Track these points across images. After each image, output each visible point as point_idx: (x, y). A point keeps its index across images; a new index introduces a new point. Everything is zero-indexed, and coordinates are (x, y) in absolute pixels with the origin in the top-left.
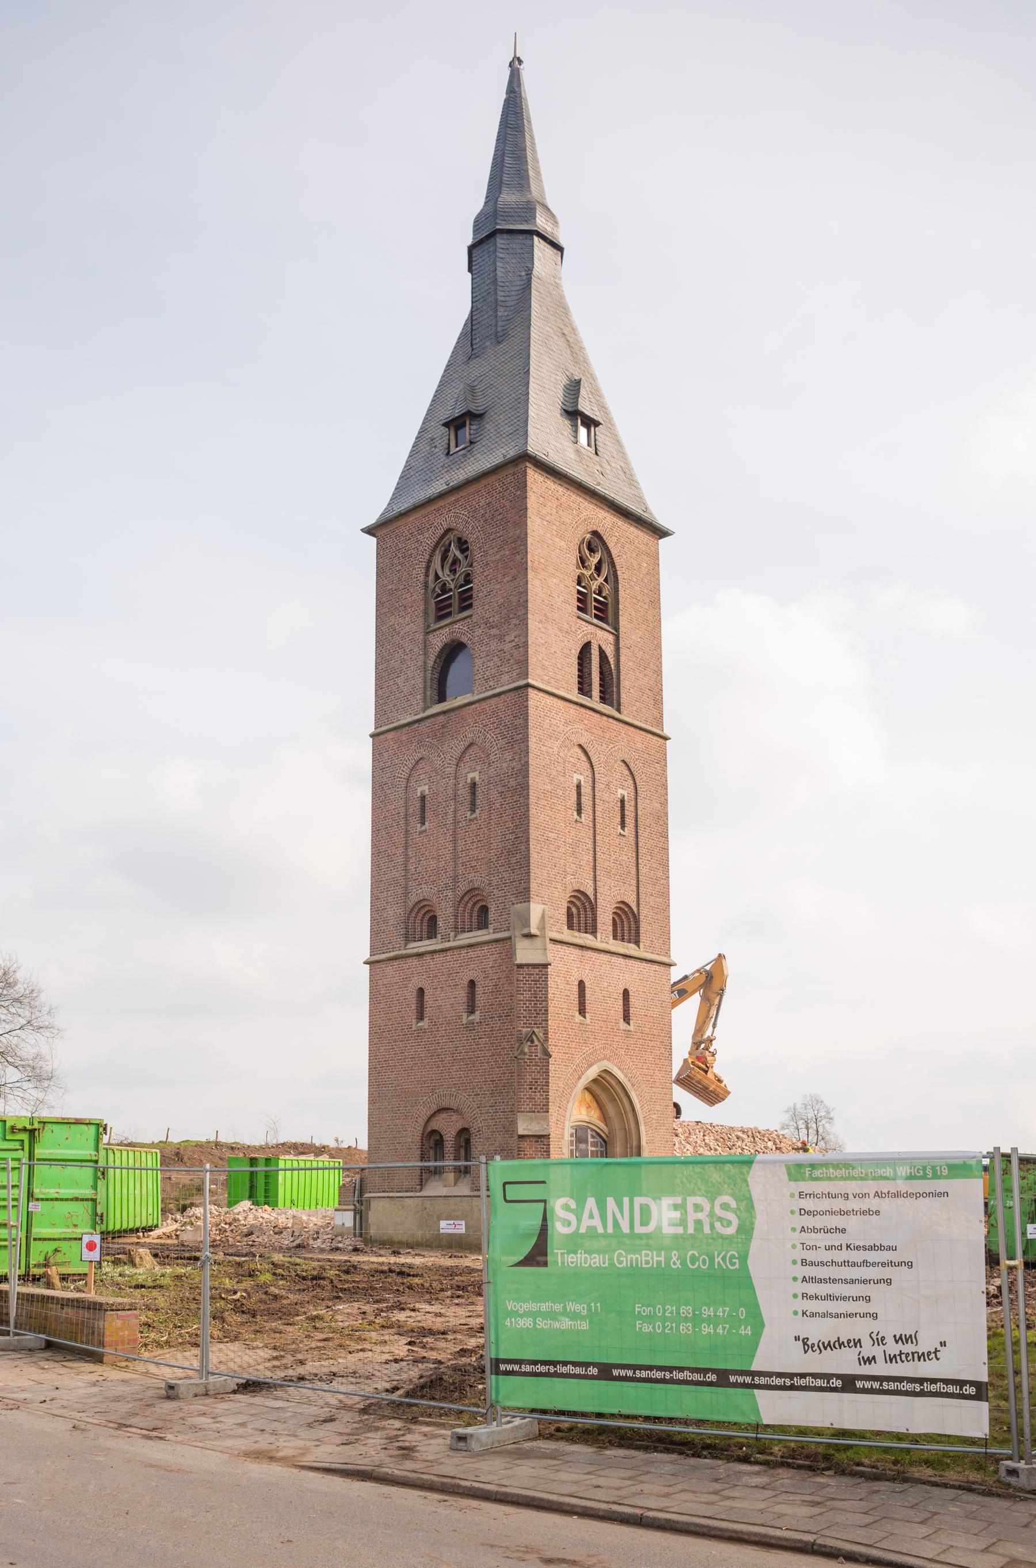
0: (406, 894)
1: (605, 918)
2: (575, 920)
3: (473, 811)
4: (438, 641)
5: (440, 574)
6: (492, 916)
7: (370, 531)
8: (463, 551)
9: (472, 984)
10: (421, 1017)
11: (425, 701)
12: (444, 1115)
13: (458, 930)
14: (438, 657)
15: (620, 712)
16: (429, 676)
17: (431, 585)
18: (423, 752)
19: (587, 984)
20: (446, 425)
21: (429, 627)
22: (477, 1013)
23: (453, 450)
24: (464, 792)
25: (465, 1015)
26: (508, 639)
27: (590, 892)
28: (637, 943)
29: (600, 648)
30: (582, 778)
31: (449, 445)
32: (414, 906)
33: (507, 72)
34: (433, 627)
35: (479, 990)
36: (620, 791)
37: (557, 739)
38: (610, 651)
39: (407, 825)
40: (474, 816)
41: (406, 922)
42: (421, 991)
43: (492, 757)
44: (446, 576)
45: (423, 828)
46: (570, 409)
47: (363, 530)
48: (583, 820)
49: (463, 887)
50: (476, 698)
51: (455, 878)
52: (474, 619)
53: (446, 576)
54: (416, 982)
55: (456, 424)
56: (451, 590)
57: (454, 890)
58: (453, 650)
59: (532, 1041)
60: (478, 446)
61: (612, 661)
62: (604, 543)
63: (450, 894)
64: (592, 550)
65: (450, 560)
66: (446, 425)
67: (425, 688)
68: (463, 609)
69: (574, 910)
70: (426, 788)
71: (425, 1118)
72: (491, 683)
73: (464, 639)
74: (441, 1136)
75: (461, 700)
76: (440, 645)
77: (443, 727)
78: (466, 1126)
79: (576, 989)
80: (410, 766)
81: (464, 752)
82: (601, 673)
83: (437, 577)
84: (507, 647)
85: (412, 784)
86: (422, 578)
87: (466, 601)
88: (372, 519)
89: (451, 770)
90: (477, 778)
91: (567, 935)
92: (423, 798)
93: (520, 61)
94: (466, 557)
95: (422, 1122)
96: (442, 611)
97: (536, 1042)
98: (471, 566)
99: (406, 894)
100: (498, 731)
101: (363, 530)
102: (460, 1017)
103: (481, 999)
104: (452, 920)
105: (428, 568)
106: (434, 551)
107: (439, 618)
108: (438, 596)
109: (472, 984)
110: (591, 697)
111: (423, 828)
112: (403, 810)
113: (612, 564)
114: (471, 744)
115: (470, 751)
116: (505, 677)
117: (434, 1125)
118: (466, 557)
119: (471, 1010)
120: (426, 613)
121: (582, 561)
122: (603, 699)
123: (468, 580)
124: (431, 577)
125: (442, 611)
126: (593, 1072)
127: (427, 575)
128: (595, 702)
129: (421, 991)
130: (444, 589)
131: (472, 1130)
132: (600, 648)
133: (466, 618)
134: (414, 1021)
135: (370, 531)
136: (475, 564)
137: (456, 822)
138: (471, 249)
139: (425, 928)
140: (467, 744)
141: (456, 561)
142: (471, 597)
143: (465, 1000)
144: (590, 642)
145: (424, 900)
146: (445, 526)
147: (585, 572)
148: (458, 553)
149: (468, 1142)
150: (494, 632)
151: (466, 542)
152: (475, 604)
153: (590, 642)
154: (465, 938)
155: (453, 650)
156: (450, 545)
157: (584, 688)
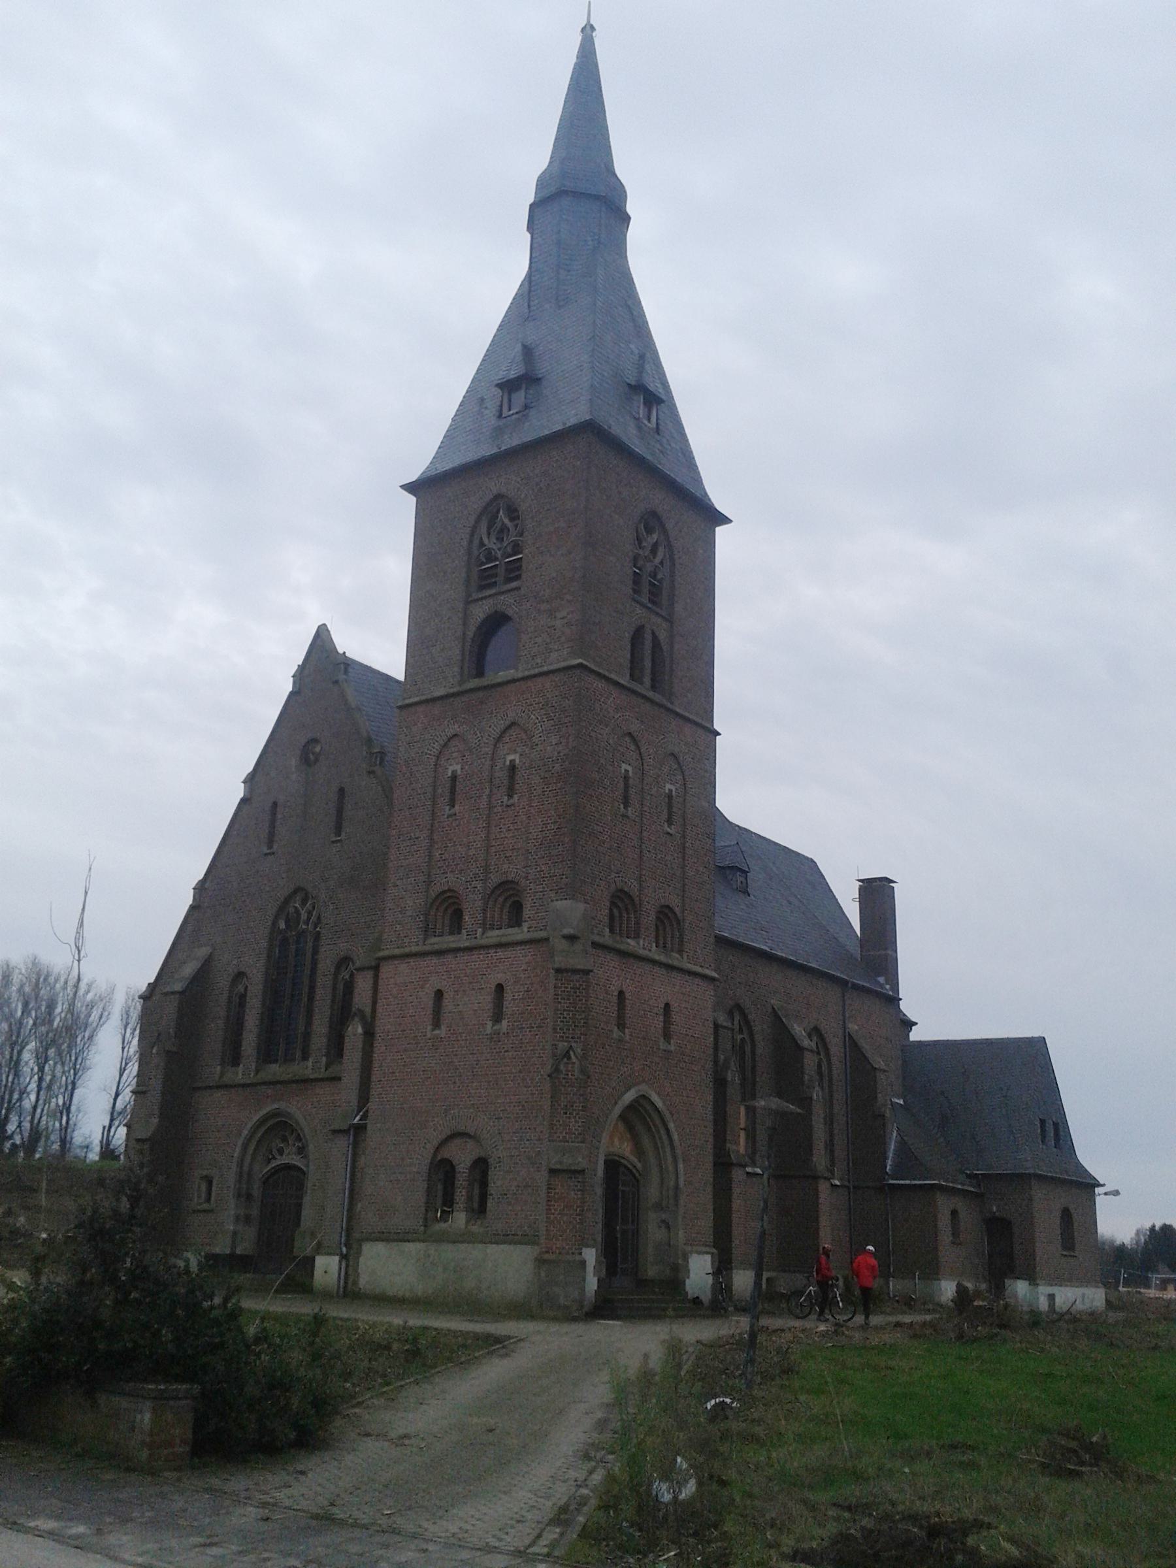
0: (429, 883)
1: (649, 919)
2: (617, 924)
3: (510, 796)
4: (480, 612)
5: (486, 541)
6: (527, 912)
7: (410, 488)
8: (512, 519)
9: (500, 988)
10: (437, 1024)
11: (462, 674)
12: (458, 1141)
13: (486, 926)
14: (479, 628)
15: (672, 703)
16: (468, 647)
17: (476, 552)
18: (455, 728)
19: (627, 995)
20: (499, 386)
21: (470, 596)
22: (504, 1022)
23: (505, 413)
24: (501, 775)
25: (490, 1024)
26: (559, 615)
27: (635, 892)
28: (680, 952)
29: (653, 633)
30: (629, 768)
31: (501, 406)
32: (437, 897)
33: (578, 39)
34: (475, 596)
35: (508, 996)
36: (668, 786)
37: (607, 726)
38: (662, 636)
39: (434, 805)
40: (511, 801)
41: (426, 915)
42: (439, 994)
43: (536, 740)
44: (491, 543)
45: (453, 811)
46: (633, 383)
47: (403, 487)
48: (629, 813)
49: (495, 879)
50: (520, 675)
51: (487, 870)
52: (523, 591)
53: (491, 543)
54: (435, 983)
55: (509, 386)
56: (496, 559)
57: (484, 881)
58: (496, 622)
59: (569, 1058)
60: (533, 412)
61: (665, 648)
62: (662, 525)
63: (479, 885)
64: (649, 530)
65: (498, 525)
66: (499, 386)
67: (462, 661)
68: (509, 580)
69: (616, 912)
70: (458, 767)
71: (436, 1143)
72: (539, 661)
73: (510, 612)
74: (453, 1167)
75: (503, 676)
76: (482, 616)
77: (482, 703)
78: (482, 1154)
79: (615, 999)
80: (442, 742)
81: (504, 731)
82: (653, 661)
83: (482, 544)
84: (558, 623)
85: (442, 762)
86: (465, 543)
87: (514, 571)
88: (413, 476)
89: (488, 750)
90: (517, 761)
91: (607, 938)
92: (454, 778)
93: (593, 28)
94: (516, 526)
95: (431, 1148)
96: (486, 580)
97: (574, 1059)
98: (521, 535)
99: (429, 883)
100: (543, 712)
101: (403, 487)
102: (484, 1025)
103: (509, 1006)
104: (480, 916)
105: (472, 535)
106: (481, 514)
107: (482, 588)
108: (483, 564)
109: (500, 988)
110: (642, 683)
111: (453, 811)
112: (430, 789)
113: (669, 546)
114: (513, 724)
115: (511, 731)
116: (554, 655)
117: (445, 1153)
118: (516, 526)
119: (498, 1017)
120: (468, 581)
121: (639, 540)
122: (653, 687)
123: (517, 548)
124: (476, 542)
125: (486, 580)
126: (629, 1096)
127: (471, 542)
128: (644, 689)
129: (439, 994)
130: (490, 557)
131: (491, 1161)
132: (653, 633)
133: (512, 590)
134: (429, 1028)
135: (410, 488)
136: (526, 534)
137: (490, 807)
138: (531, 206)
139: (447, 922)
140: (507, 723)
141: (504, 529)
142: (519, 568)
143: (491, 1006)
144: (643, 626)
145: (449, 890)
146: (495, 492)
147: (641, 552)
148: (506, 521)
149: (485, 1174)
150: (544, 606)
151: (516, 510)
152: (524, 576)
153: (643, 626)
154: (494, 936)
155: (496, 622)
156: (498, 512)
157: (635, 672)
